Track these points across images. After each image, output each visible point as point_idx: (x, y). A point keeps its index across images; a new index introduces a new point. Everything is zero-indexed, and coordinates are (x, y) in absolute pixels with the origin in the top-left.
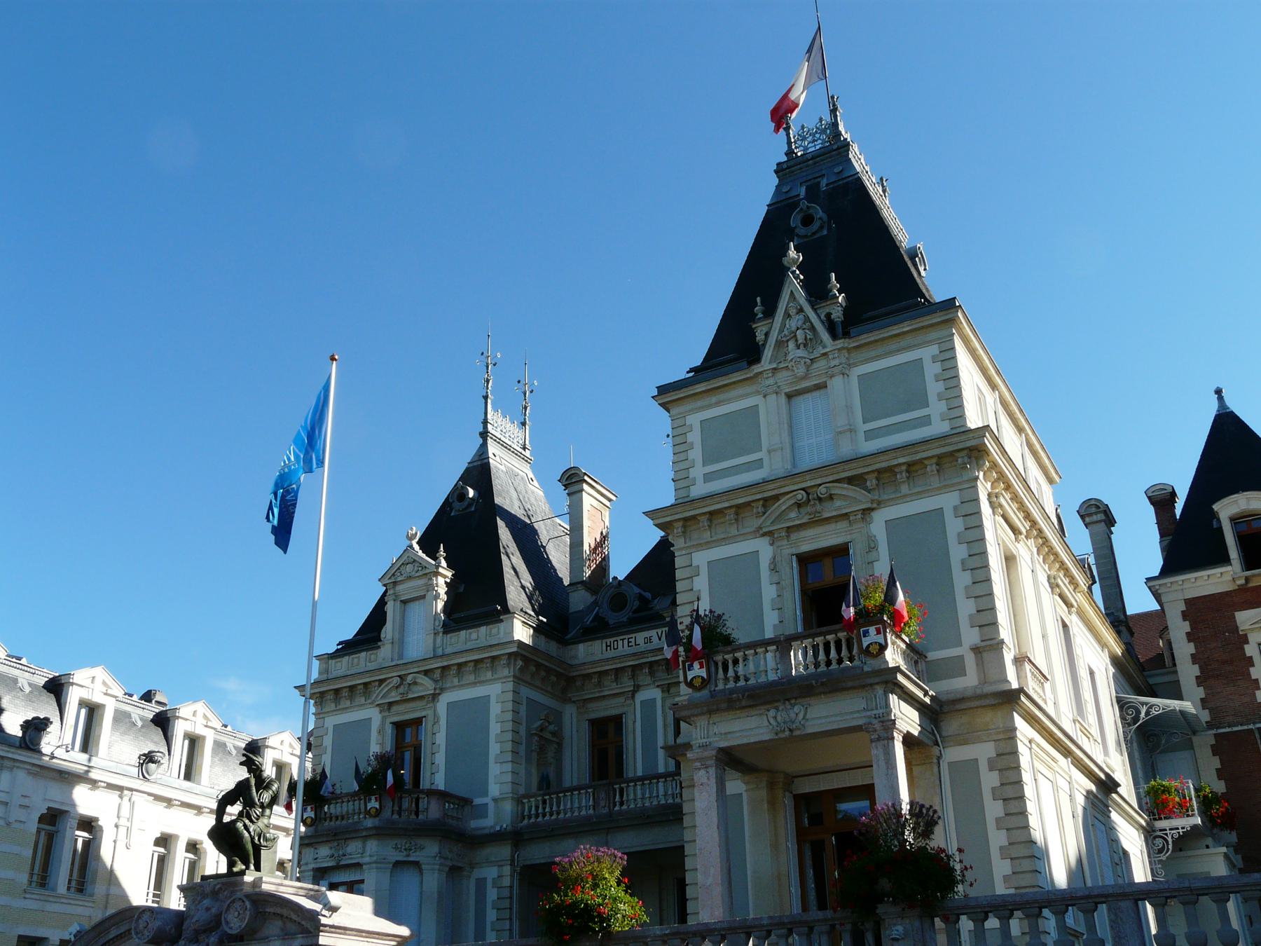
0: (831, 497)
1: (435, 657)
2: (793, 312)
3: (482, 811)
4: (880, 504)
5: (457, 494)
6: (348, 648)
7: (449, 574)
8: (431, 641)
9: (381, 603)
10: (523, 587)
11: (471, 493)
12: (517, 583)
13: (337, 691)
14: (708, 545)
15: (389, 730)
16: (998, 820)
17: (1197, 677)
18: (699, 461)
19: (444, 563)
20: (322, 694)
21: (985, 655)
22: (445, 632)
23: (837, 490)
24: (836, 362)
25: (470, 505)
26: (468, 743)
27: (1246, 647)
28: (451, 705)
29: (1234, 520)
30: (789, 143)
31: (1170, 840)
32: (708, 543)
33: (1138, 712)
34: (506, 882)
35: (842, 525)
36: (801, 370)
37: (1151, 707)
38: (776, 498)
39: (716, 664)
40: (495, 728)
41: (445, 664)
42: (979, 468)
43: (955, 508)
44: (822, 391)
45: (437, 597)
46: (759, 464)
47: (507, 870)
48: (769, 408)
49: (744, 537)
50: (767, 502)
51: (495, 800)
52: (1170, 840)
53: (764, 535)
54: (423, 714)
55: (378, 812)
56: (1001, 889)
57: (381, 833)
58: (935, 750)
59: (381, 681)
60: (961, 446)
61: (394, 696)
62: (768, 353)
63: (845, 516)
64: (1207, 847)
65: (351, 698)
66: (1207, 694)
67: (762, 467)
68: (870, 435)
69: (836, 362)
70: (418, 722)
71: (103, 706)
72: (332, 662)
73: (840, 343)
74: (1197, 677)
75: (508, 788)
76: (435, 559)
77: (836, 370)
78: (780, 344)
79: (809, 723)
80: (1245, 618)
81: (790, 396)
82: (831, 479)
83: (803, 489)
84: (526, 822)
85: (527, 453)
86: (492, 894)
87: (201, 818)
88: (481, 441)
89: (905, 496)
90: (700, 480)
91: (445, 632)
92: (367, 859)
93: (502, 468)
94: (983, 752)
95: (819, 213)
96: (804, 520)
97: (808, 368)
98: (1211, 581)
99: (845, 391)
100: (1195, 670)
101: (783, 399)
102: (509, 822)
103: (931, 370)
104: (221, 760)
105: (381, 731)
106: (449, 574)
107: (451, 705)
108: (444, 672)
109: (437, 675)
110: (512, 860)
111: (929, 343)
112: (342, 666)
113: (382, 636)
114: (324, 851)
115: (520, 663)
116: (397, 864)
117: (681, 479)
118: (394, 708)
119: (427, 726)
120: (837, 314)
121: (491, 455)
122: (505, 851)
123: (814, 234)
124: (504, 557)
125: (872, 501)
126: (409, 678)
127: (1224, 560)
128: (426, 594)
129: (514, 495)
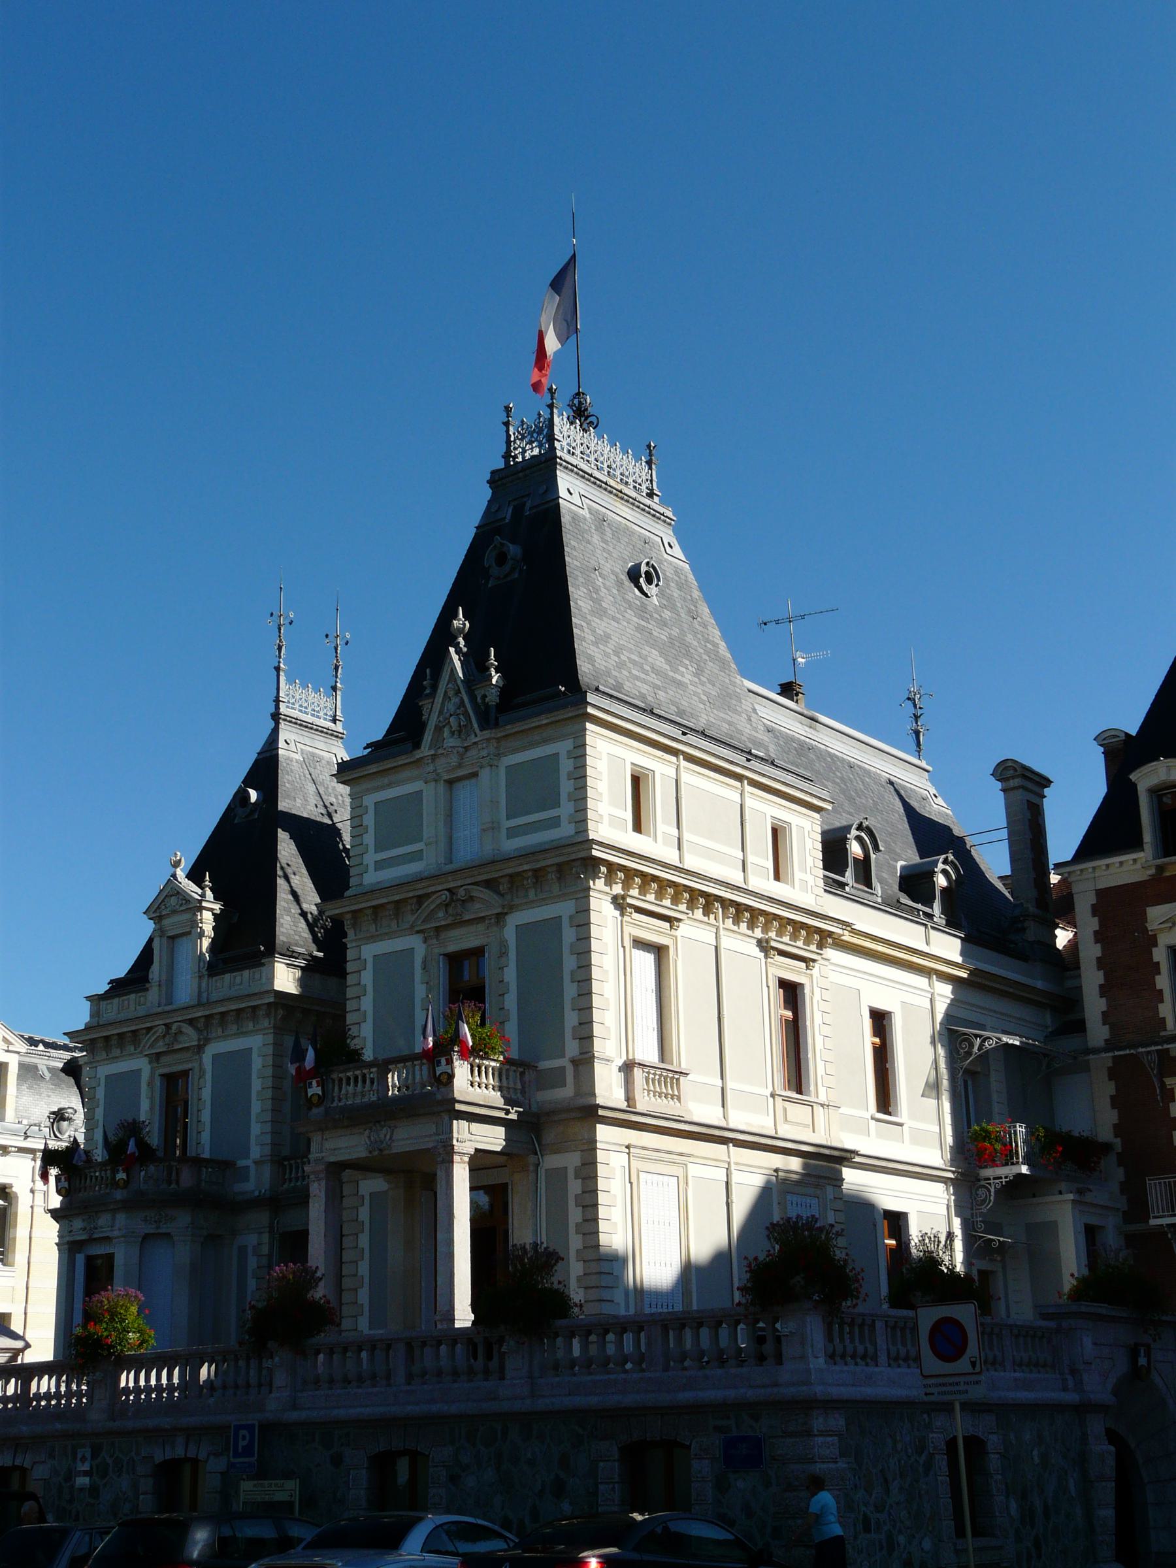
1: (199, 1004)
2: (451, 693)
3: (243, 1174)
4: (512, 908)
5: (241, 797)
6: (118, 987)
7: (217, 907)
8: (196, 985)
9: (151, 940)
10: (304, 914)
11: (253, 795)
12: (295, 910)
13: (107, 1038)
14: (373, 938)
15: (158, 1082)
16: (577, 1225)
17: (1101, 986)
18: (371, 848)
19: (209, 895)
20: (93, 1041)
21: (580, 1068)
22: (211, 975)
23: (477, 892)
24: (484, 753)
25: (252, 812)
26: (231, 1101)
27: (1154, 950)
28: (215, 1057)
29: (1156, 792)
30: (508, 442)
31: (993, 1190)
32: (372, 937)
33: (972, 1045)
34: (265, 1250)
35: (481, 927)
36: (454, 760)
37: (984, 1041)
38: (428, 895)
39: (333, 1081)
40: (256, 1084)
41: (207, 1013)
42: (595, 876)
43: (571, 917)
44: (473, 780)
45: (202, 934)
46: (417, 856)
47: (266, 1238)
48: (431, 795)
50: (420, 899)
51: (256, 1163)
52: (993, 1190)
53: (418, 932)
54: (189, 1066)
55: (127, 1183)
57: (128, 1206)
58: (532, 1159)
59: (149, 1029)
60: (573, 857)
61: (160, 1047)
62: (428, 737)
63: (483, 919)
64: (1060, 1193)
65: (121, 1046)
66: (1109, 1006)
67: (421, 859)
68: (512, 833)
69: (484, 753)
72: (103, 1004)
73: (487, 734)
74: (1101, 986)
75: (267, 1150)
76: (202, 888)
77: (486, 761)
78: (439, 729)
79: (395, 1144)
80: (1156, 914)
81: (450, 783)
82: (469, 881)
83: (448, 890)
84: (285, 1186)
85: (339, 727)
86: (252, 1263)
87: (8, 1158)
88: (273, 724)
89: (533, 901)
90: (371, 868)
91: (211, 975)
92: (116, 1233)
93: (585, 513)
95: (514, 550)
96: (448, 922)
97: (462, 756)
98: (1125, 868)
99: (491, 785)
100: (1098, 978)
101: (441, 787)
102: (267, 1186)
103: (566, 765)
104: (30, 1088)
105: (150, 1084)
106: (217, 907)
107: (215, 1057)
108: (210, 1021)
109: (200, 1025)
110: (271, 1227)
112: (111, 1011)
113: (150, 976)
114: (78, 1224)
115: (281, 1012)
116: (146, 1237)
118: (164, 1059)
119: (193, 1078)
120: (493, 697)
121: (563, 493)
122: (261, 1218)
123: (506, 576)
124: (280, 882)
125: (503, 906)
126: (174, 1027)
127: (1136, 844)
128: (192, 930)
129: (311, 789)
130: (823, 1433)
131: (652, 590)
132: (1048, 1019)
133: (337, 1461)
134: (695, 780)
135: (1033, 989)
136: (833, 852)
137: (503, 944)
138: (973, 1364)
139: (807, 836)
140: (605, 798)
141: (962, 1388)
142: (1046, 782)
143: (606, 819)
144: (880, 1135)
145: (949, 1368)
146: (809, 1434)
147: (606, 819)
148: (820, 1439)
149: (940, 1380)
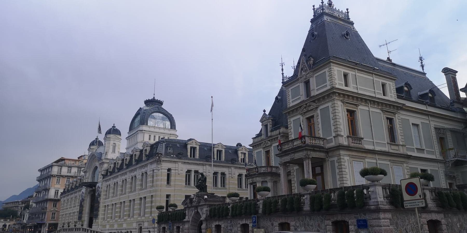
0: (310, 105)
18: (327, 72)
49: (296, 115)
56: (338, 187)
68: (317, 90)
70: (313, 117)
71: (196, 147)
94: (335, 159)
111: (327, 68)
117: (330, 71)
119: (315, 118)
130: (384, 219)
131: (348, 37)
132: (463, 125)
133: (272, 225)
134: (359, 74)
135: (458, 118)
136: (399, 90)
137: (318, 114)
138: (420, 196)
139: (391, 87)
140: (337, 79)
141: (417, 203)
142: (457, 72)
143: (338, 84)
144: (417, 152)
145: (412, 198)
146: (380, 219)
147: (338, 84)
148: (383, 220)
149: (410, 202)
